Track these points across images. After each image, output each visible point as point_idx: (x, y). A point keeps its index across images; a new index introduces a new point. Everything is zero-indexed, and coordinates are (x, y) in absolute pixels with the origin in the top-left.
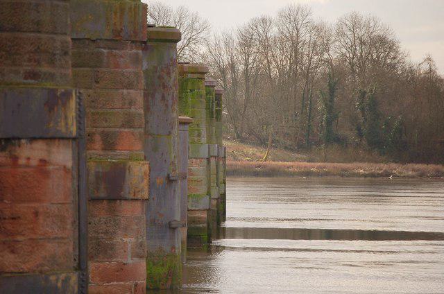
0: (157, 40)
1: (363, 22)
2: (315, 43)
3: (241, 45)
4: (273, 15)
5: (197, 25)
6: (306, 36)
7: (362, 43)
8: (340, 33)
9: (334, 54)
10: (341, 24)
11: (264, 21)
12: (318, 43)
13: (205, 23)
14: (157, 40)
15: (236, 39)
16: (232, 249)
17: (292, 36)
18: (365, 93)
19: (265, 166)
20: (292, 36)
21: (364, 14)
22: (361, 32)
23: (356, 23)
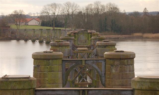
0: (101, 39)
1: (112, 4)
2: (102, 9)
3: (86, 10)
4: (93, 3)
5: (77, 6)
6: (100, 8)
7: (112, 8)
8: (107, 7)
9: (106, 11)
10: (107, 5)
11: (91, 4)
12: (103, 9)
13: (79, 5)
14: (101, 39)
15: (85, 8)
16: (17, 27)
17: (97, 8)
18: (113, 20)
19: (108, 48)
20: (97, 8)
21: (112, 3)
22: (111, 6)
23: (110, 4)
